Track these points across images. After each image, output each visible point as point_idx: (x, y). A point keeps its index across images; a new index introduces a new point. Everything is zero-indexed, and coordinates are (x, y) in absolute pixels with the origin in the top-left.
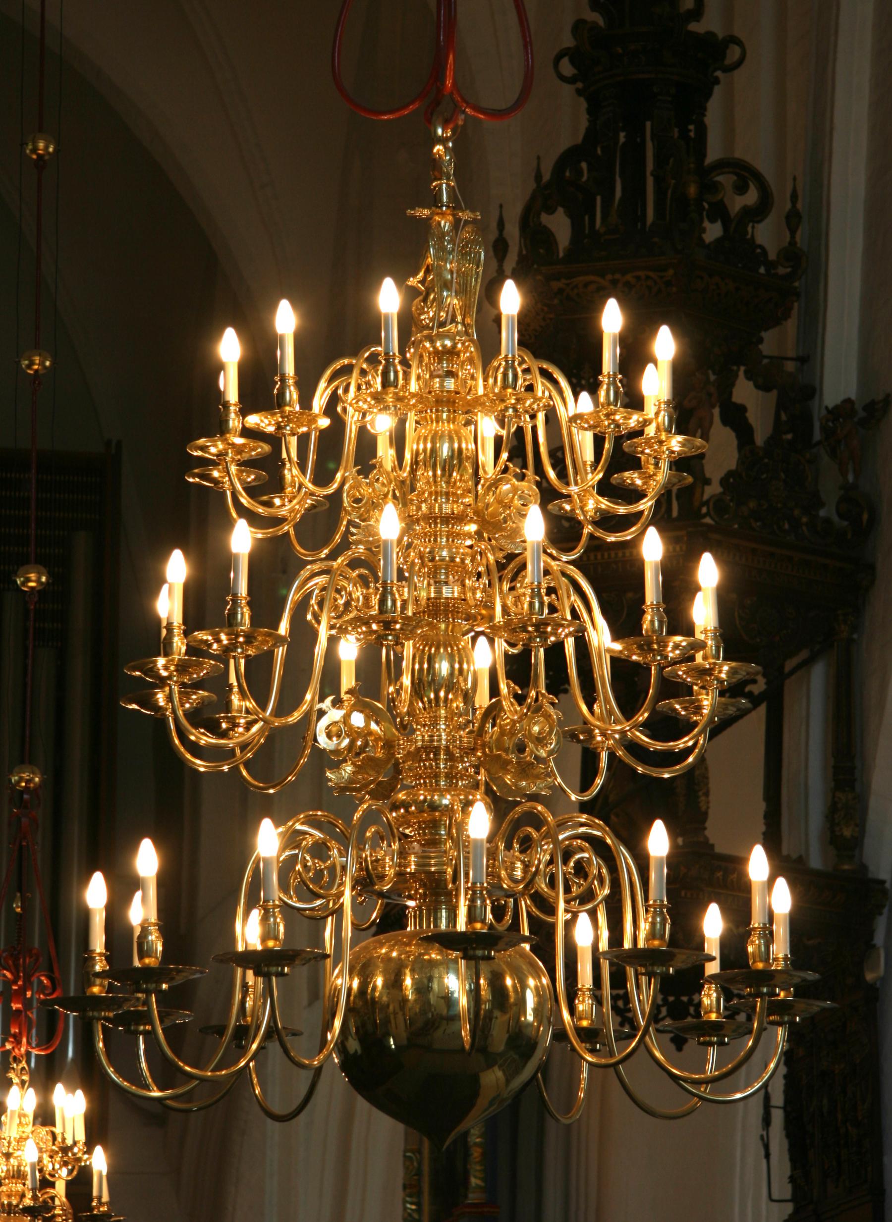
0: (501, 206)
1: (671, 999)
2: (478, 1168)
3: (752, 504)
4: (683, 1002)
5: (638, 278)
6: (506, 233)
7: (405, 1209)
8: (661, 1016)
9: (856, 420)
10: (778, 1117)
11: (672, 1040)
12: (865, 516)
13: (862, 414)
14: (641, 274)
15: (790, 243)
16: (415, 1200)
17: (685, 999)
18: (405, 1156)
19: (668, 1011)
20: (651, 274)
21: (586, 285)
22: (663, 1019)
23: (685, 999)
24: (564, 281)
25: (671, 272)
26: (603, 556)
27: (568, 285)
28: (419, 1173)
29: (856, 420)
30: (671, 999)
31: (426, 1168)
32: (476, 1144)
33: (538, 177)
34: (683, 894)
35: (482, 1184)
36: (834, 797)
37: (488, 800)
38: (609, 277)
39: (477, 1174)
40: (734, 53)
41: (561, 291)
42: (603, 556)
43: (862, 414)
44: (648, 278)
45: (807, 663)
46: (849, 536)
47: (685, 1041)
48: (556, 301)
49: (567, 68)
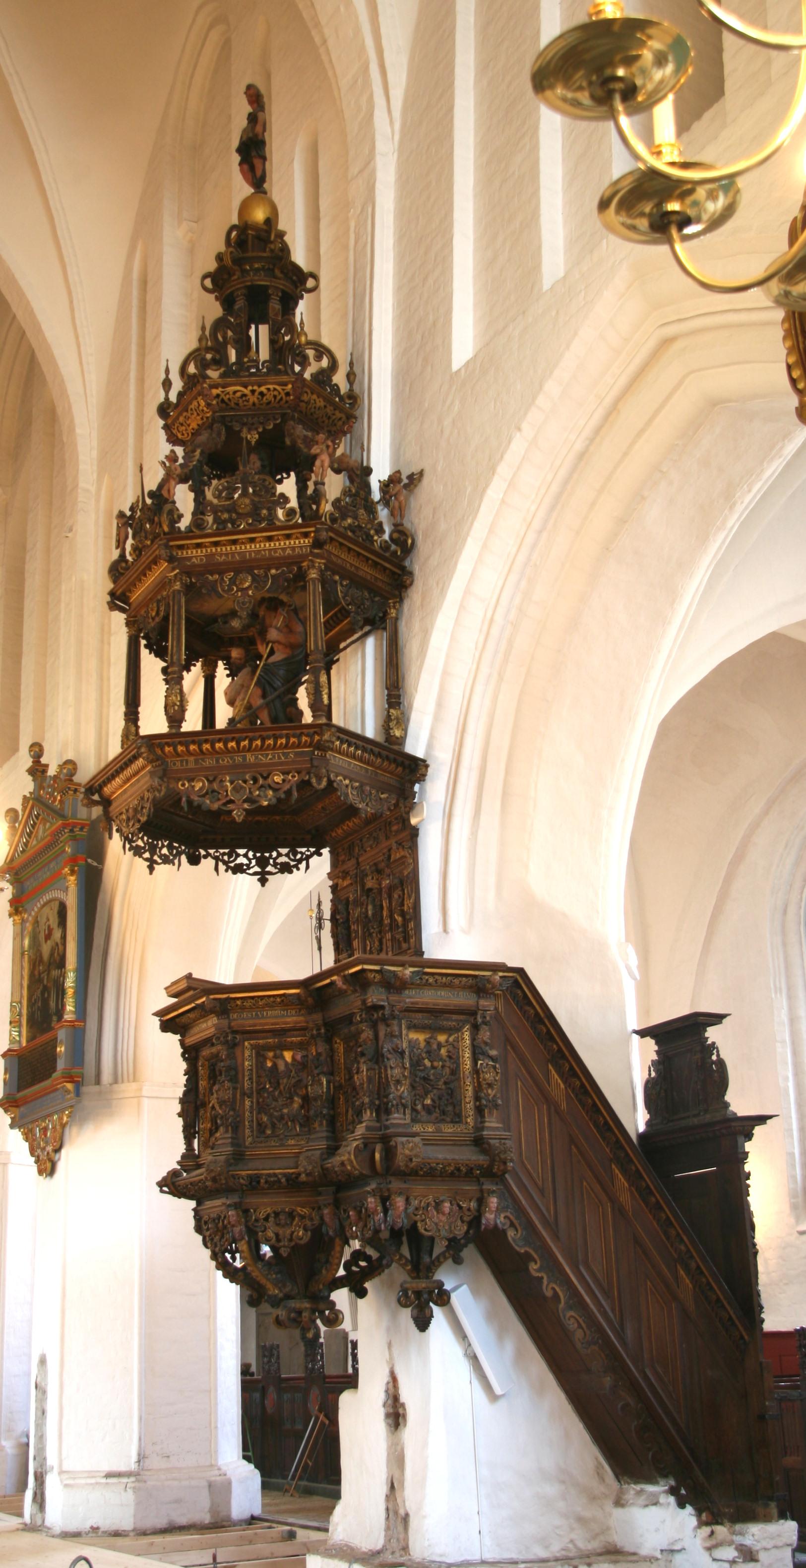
0: (167, 361)
1: (258, 855)
2: (71, 1000)
3: (349, 521)
4: (266, 856)
5: (269, 389)
6: (170, 376)
7: (11, 1035)
8: (251, 865)
9: (402, 484)
10: (328, 925)
11: (259, 880)
12: (410, 541)
13: (405, 481)
14: (271, 387)
15: (349, 390)
16: (17, 1029)
17: (267, 855)
18: (11, 1005)
19: (256, 862)
20: (277, 387)
21: (235, 392)
22: (253, 867)
23: (267, 855)
24: (220, 389)
25: (290, 386)
26: (255, 546)
27: (223, 392)
28: (20, 1015)
29: (402, 484)
30: (258, 855)
31: (25, 1012)
32: (70, 987)
33: (203, 328)
34: (316, 753)
35: (73, 1009)
36: (389, 712)
37: (717, 215)
38: (250, 388)
39: (71, 1004)
40: (310, 283)
41: (218, 396)
42: (255, 546)
43: (405, 481)
44: (275, 389)
45: (366, 635)
46: (399, 553)
47: (267, 880)
48: (214, 402)
49: (208, 283)
